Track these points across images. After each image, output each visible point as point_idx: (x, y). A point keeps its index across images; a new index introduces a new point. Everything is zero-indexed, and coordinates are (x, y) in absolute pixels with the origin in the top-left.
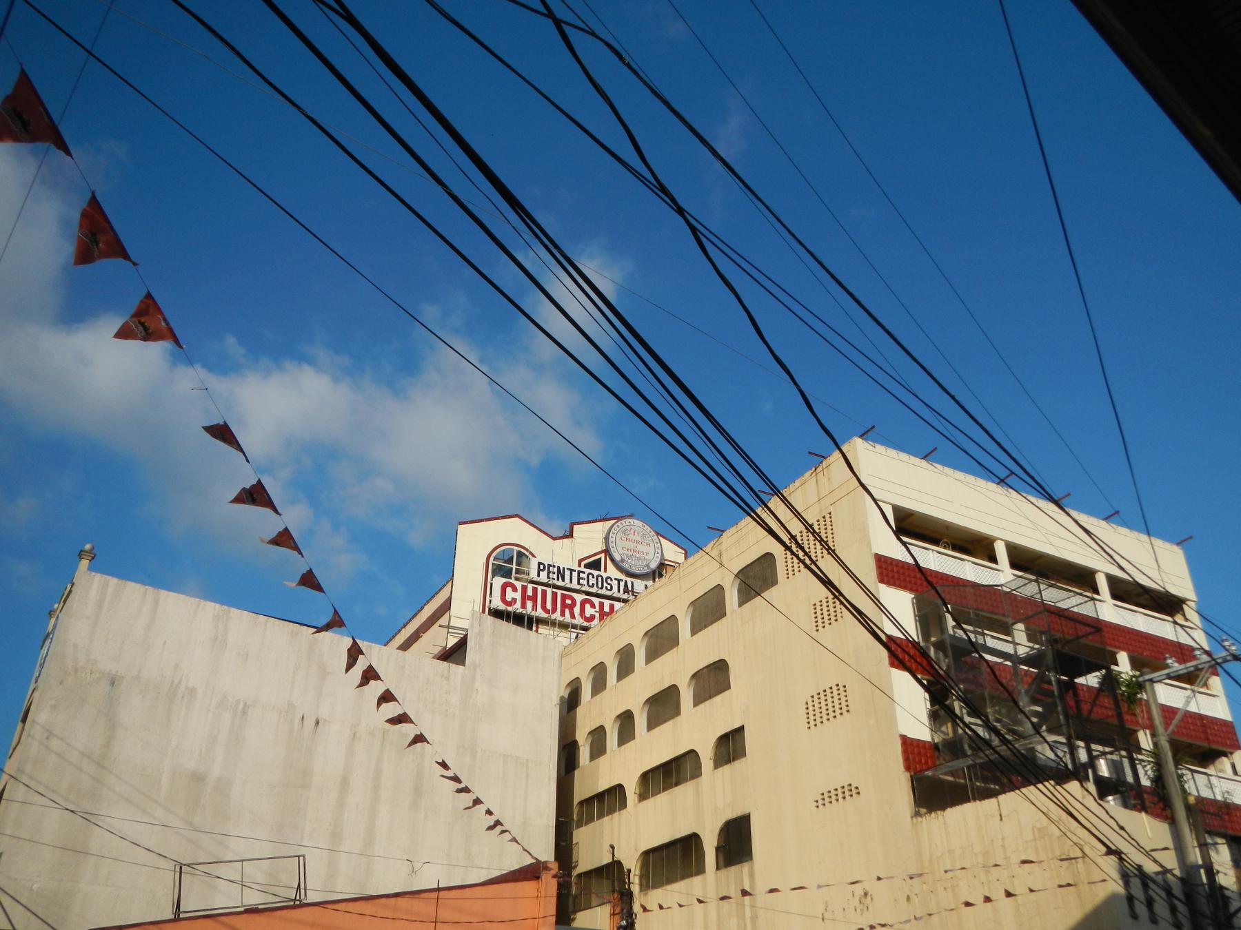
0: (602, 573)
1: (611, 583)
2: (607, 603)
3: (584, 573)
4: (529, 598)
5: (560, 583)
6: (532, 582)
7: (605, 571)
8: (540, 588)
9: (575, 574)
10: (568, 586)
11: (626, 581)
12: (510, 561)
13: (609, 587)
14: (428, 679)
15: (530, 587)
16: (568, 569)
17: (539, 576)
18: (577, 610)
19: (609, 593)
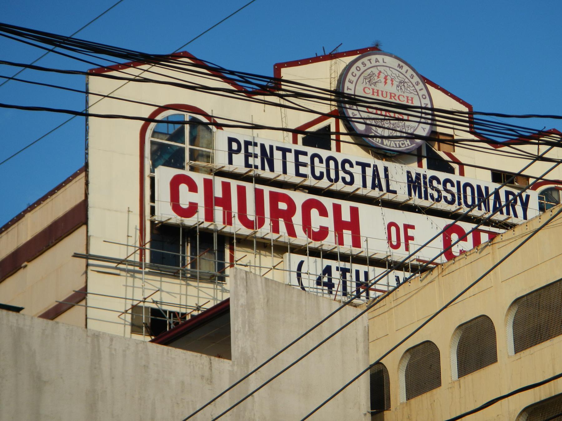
0: (333, 153)
1: (351, 170)
2: (346, 206)
3: (305, 154)
4: (219, 202)
5: (267, 174)
6: (220, 173)
7: (338, 149)
8: (234, 184)
9: (290, 157)
10: (282, 178)
11: (375, 166)
12: (178, 136)
13: (348, 179)
14: (183, 383)
15: (218, 182)
16: (278, 149)
17: (230, 162)
18: (297, 219)
19: (349, 189)
